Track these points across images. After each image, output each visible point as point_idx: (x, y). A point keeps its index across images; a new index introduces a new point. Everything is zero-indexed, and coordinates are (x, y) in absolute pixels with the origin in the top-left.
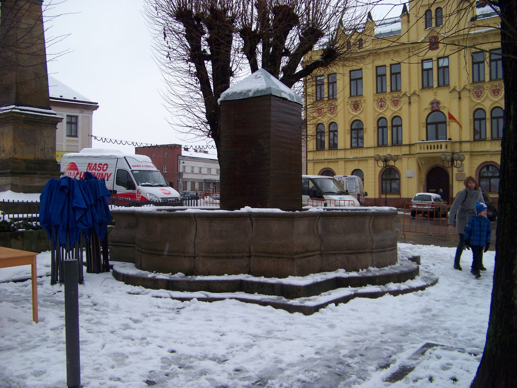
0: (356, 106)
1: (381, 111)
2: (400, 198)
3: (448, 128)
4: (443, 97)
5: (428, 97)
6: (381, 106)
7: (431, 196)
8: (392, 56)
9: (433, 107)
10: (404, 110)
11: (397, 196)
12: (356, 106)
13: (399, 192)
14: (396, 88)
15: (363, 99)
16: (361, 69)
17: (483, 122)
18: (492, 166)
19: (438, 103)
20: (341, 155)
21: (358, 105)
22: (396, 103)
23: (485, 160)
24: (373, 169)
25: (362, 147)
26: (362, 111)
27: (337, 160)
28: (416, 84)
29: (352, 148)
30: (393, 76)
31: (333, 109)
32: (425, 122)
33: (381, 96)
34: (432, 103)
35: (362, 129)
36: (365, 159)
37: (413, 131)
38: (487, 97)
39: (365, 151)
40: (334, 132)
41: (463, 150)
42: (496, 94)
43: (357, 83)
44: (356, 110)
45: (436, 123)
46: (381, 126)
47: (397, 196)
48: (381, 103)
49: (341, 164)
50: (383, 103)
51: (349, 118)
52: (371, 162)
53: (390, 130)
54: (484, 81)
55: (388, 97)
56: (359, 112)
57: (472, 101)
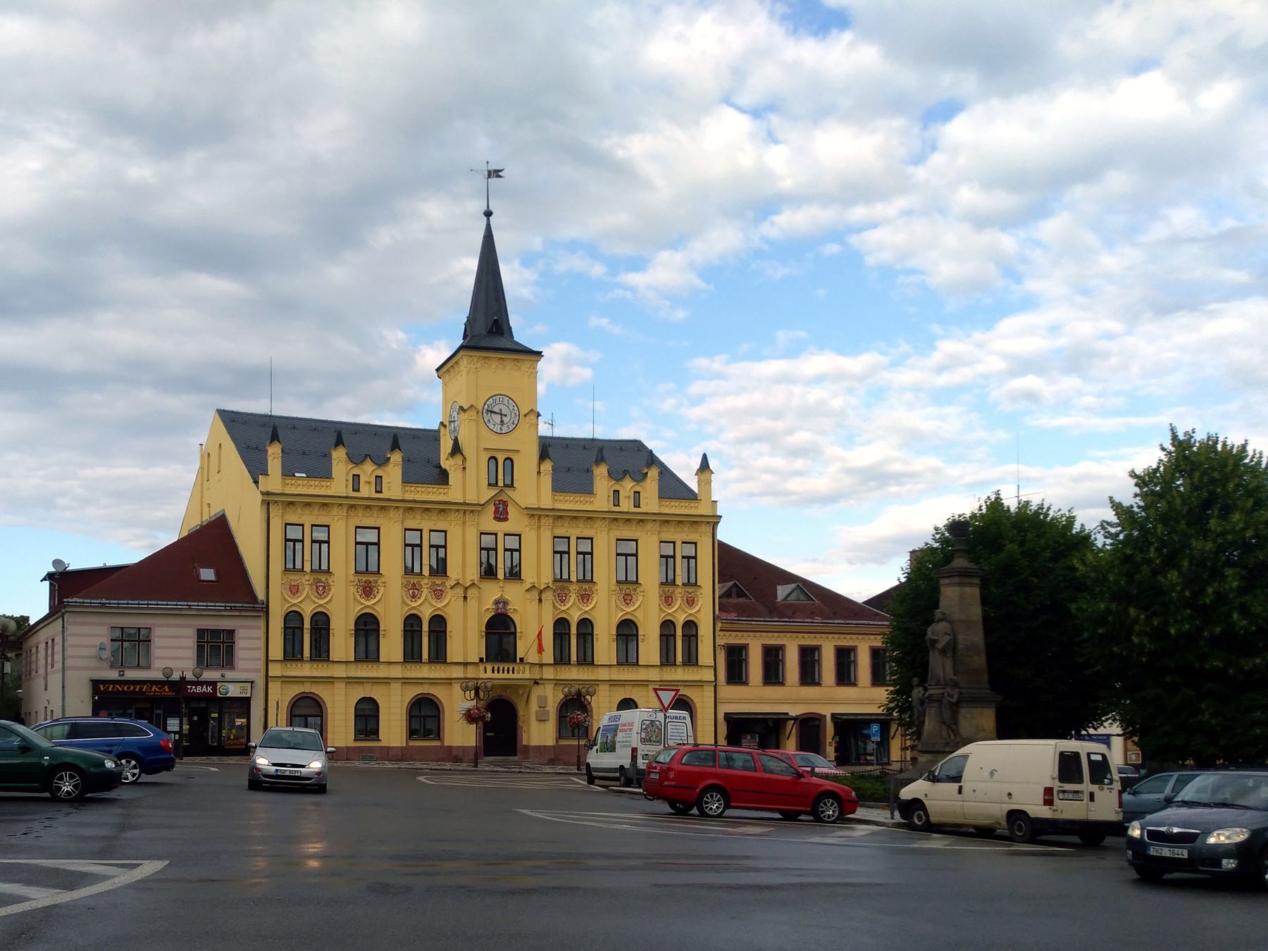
0: (368, 591)
1: (321, 602)
2: (442, 747)
5: (492, 592)
6: (414, 596)
7: (1076, 756)
8: (316, 512)
10: (451, 607)
12: (368, 591)
13: (438, 737)
14: (440, 569)
15: (383, 579)
19: (506, 603)
21: (371, 589)
22: (438, 594)
25: (592, 664)
27: (330, 680)
28: (473, 573)
29: (357, 660)
31: (322, 589)
33: (414, 580)
34: (497, 602)
36: (386, 681)
37: (466, 641)
38: (307, 596)
39: (382, 667)
41: (545, 677)
45: (500, 633)
46: (412, 624)
47: (437, 743)
48: (668, 600)
49: (340, 688)
51: (357, 610)
52: (457, 689)
53: (424, 638)
54: (569, 580)
55: (679, 592)
57: (285, 599)
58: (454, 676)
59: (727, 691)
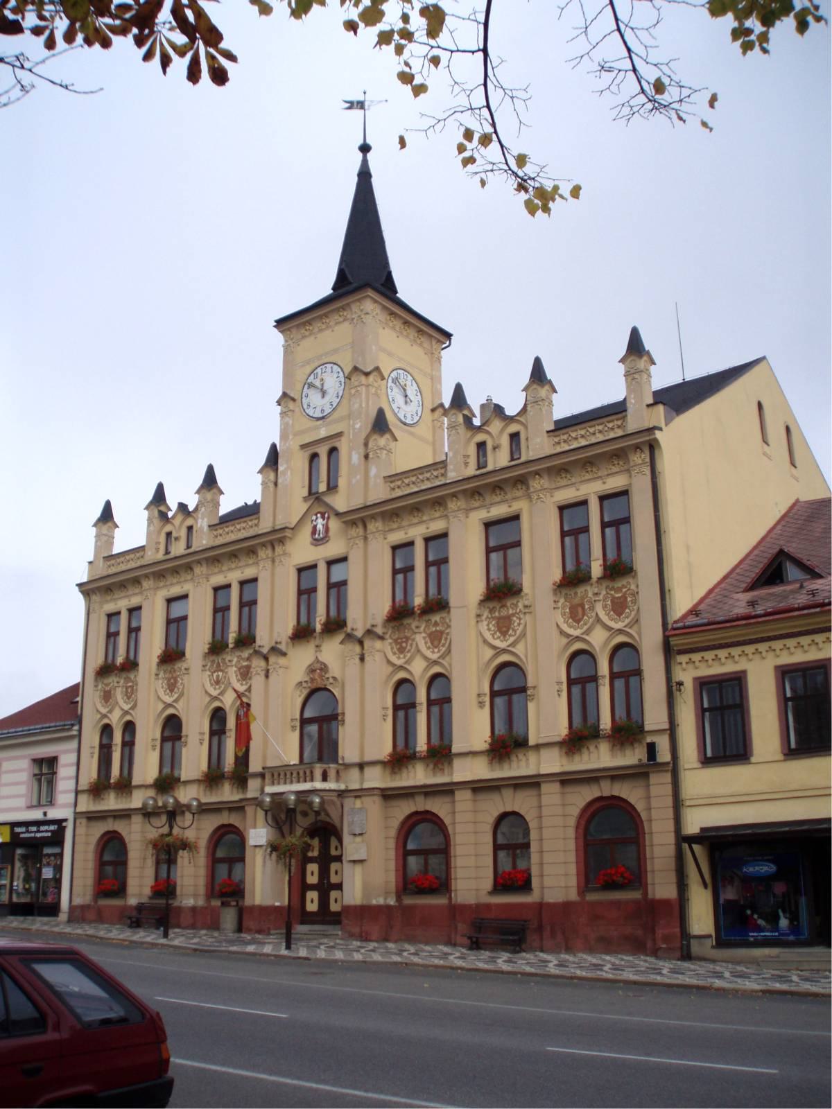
3: (340, 727)
4: (332, 652)
5: (301, 659)
6: (218, 682)
9: (312, 680)
11: (635, 895)
16: (516, 518)
17: (590, 687)
18: (101, 855)
20: (464, 771)
23: (413, 809)
24: (654, 803)
26: (181, 695)
30: (567, 540)
32: (298, 716)
35: (523, 690)
36: (532, 783)
39: (532, 757)
40: (441, 703)
42: (436, 643)
43: (178, 626)
44: (619, 614)
47: (635, 895)
50: (220, 674)
56: (512, 639)
58: (457, 778)
59: (701, 782)
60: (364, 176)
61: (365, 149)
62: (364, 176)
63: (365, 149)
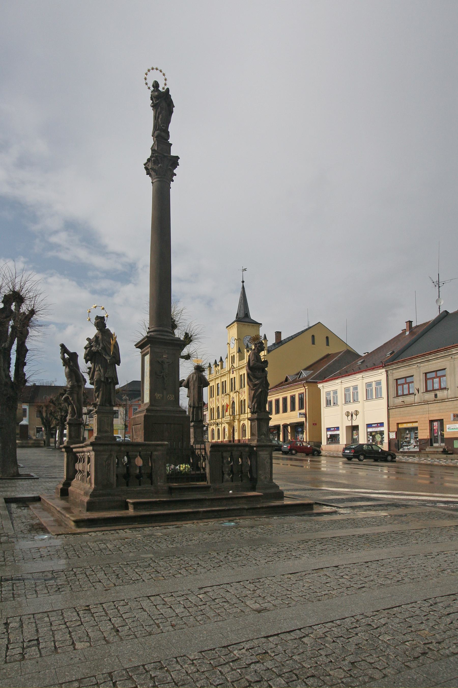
60: (243, 288)
61: (243, 282)
62: (243, 288)
63: (243, 282)
